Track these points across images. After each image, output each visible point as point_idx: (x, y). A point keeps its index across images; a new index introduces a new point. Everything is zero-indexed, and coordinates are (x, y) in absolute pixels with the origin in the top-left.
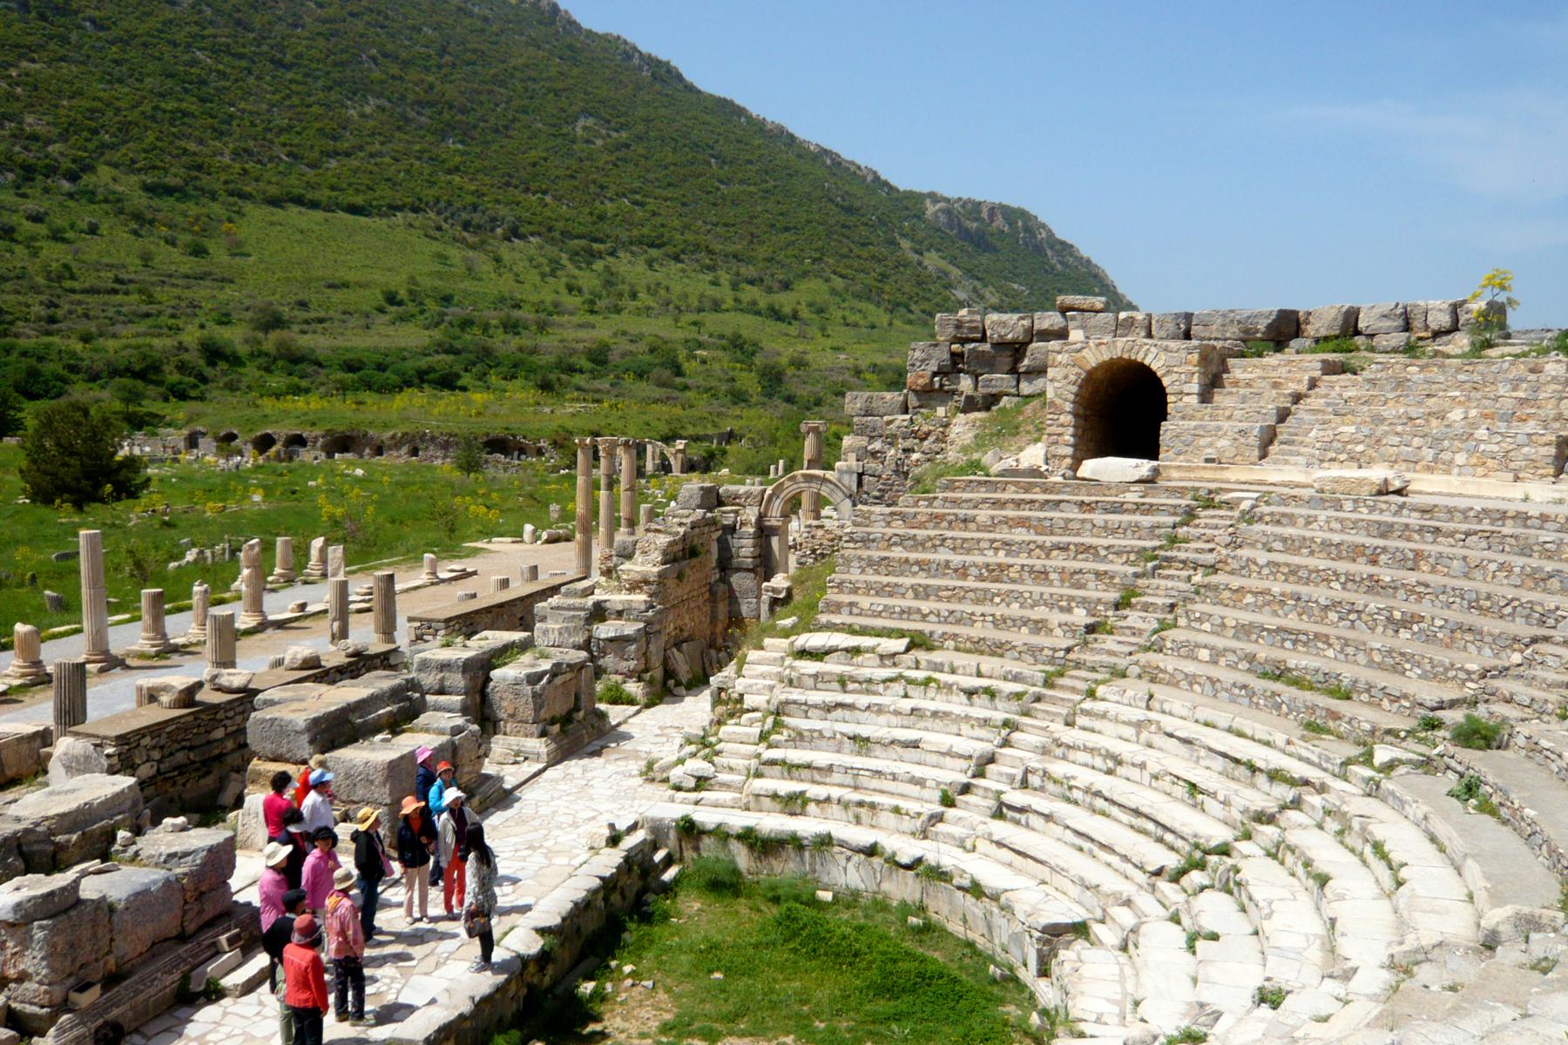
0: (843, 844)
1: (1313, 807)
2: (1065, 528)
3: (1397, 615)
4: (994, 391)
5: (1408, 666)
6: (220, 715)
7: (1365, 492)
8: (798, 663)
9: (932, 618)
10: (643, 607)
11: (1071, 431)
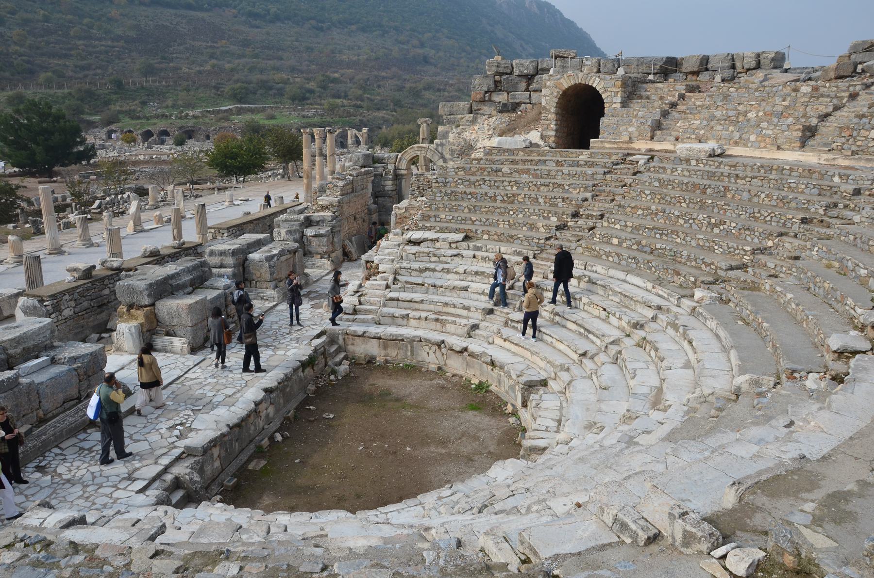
0: (426, 340)
1: (662, 321)
2: (548, 175)
3: (713, 221)
4: (517, 101)
5: (716, 247)
6: (106, 282)
7: (702, 156)
8: (407, 247)
9: (477, 223)
10: (330, 219)
11: (554, 122)
